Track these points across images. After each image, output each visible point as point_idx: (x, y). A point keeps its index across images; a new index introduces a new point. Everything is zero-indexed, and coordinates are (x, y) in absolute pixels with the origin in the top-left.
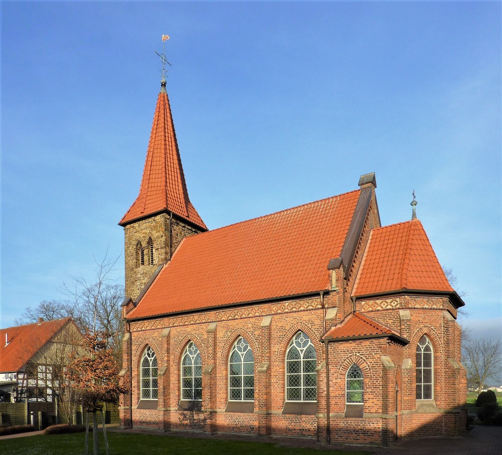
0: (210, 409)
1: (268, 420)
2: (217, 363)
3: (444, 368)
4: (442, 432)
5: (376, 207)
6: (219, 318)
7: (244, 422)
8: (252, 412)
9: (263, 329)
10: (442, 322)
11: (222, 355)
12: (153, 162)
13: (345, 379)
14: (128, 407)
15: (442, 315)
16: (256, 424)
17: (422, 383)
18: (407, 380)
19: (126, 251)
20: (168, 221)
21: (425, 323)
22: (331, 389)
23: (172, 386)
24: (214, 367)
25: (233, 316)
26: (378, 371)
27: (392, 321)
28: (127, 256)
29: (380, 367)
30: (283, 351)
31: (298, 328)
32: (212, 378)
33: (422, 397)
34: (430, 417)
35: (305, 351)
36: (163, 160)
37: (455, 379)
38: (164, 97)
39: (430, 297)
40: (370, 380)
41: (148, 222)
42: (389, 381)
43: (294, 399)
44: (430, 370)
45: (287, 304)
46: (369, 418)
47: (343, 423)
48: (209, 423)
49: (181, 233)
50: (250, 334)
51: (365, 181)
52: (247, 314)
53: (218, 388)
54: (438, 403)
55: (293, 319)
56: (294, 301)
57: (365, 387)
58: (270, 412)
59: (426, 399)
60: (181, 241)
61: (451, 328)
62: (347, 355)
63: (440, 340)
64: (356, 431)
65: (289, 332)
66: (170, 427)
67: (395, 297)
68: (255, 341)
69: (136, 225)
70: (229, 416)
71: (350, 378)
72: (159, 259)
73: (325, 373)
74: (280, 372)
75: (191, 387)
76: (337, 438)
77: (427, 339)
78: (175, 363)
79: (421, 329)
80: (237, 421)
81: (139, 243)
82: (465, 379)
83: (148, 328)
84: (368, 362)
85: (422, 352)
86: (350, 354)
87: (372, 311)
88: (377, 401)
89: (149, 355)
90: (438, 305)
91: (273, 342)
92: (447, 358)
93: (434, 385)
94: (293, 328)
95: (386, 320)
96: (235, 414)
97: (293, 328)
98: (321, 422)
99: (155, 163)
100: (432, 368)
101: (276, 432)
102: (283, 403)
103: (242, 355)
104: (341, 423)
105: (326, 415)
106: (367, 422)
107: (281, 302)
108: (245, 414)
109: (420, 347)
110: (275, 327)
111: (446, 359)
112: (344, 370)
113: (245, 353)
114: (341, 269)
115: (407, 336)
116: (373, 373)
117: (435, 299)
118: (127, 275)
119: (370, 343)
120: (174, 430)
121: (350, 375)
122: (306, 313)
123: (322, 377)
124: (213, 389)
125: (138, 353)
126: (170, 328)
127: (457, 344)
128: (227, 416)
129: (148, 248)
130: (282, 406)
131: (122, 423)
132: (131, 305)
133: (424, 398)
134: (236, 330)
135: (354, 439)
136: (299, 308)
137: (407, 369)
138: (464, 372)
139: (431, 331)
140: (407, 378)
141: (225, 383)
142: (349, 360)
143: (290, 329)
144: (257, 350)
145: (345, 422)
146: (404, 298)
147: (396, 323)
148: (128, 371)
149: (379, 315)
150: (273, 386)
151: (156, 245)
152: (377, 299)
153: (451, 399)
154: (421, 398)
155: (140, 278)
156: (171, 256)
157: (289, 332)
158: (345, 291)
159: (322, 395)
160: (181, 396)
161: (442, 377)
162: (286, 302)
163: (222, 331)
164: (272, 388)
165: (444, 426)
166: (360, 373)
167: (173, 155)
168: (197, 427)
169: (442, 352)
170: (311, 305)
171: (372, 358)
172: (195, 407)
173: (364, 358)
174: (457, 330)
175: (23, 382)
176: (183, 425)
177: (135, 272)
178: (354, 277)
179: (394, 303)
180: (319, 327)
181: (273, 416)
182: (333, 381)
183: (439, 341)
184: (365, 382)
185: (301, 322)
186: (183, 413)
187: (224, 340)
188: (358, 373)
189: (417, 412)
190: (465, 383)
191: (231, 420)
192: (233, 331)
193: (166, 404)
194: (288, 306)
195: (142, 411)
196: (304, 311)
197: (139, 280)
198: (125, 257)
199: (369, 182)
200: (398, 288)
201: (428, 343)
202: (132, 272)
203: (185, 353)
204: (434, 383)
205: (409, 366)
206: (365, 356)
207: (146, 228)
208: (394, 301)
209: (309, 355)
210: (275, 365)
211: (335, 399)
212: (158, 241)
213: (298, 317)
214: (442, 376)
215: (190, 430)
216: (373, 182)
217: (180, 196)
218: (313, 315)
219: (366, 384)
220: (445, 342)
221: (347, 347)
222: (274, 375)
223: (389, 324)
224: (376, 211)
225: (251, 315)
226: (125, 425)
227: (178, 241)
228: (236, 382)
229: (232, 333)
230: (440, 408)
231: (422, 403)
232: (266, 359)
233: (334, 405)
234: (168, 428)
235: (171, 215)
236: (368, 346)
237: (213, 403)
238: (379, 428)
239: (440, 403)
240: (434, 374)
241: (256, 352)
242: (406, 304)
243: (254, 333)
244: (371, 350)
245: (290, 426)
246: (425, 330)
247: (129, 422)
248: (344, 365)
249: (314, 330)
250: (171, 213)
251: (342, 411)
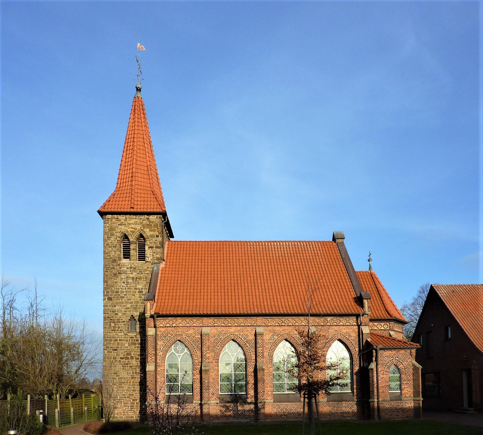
11: (268, 355)
22: (380, 382)
45: (329, 319)
69: (122, 218)
72: (153, 257)
76: (384, 416)
86: (392, 359)
96: (283, 403)
113: (182, 354)
118: (107, 265)
136: (339, 323)
155: (126, 271)
170: (348, 322)
176: (226, 416)
179: (386, 326)
182: (381, 376)
186: (225, 405)
192: (280, 335)
194: (330, 321)
196: (343, 325)
197: (125, 273)
202: (115, 264)
233: (382, 392)
248: (388, 366)
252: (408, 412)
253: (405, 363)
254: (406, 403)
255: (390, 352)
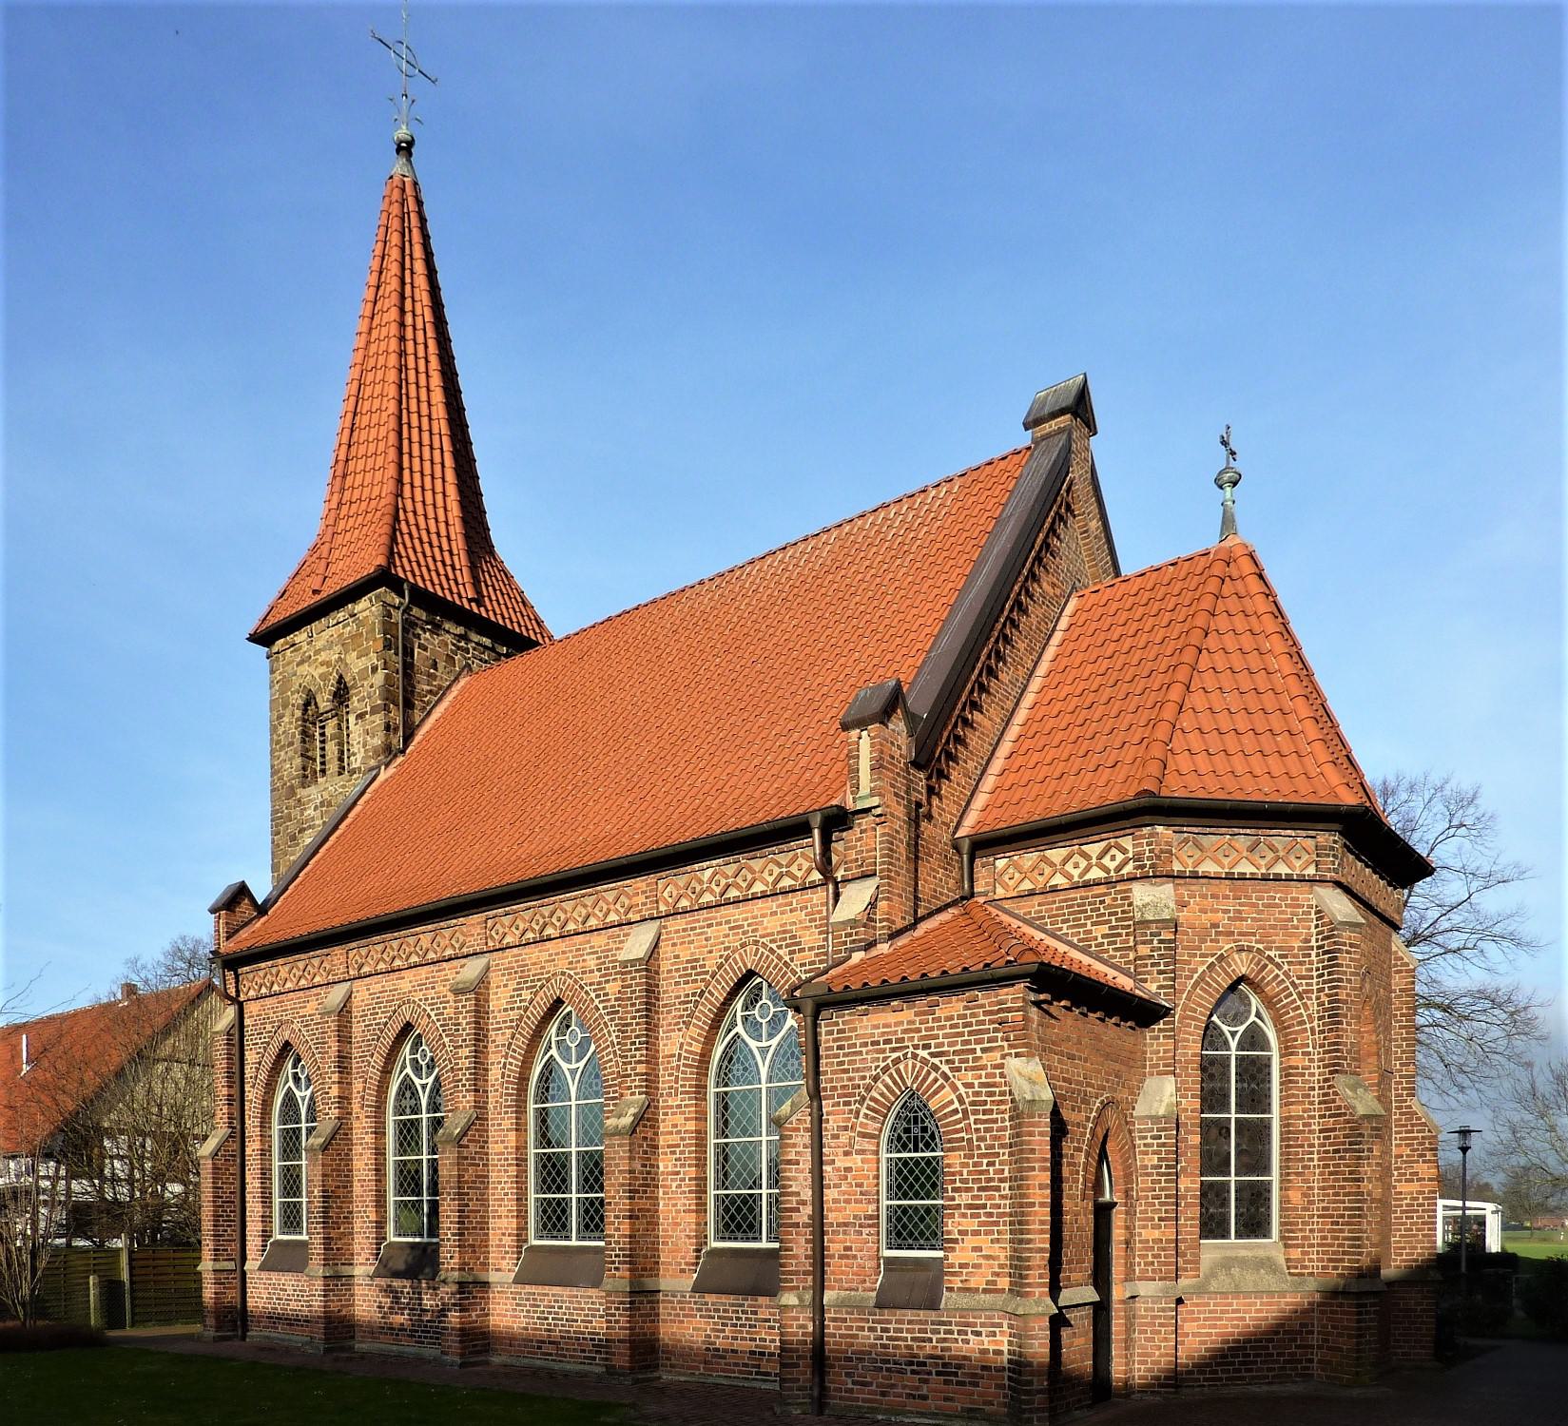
0: (456, 1273)
1: (641, 1316)
2: (490, 1106)
3: (1321, 1117)
4: (1308, 1368)
5: (1094, 507)
6: (496, 937)
7: (559, 1319)
8: (596, 1284)
9: (626, 973)
10: (1314, 931)
11: (503, 1073)
12: (358, 418)
13: (877, 1153)
14: (231, 1265)
15: (1314, 903)
16: (599, 1325)
17: (1229, 1175)
18: (1156, 1162)
19: (274, 729)
20: (397, 616)
21: (1241, 934)
22: (830, 1194)
23: (357, 1189)
24: (477, 1118)
25: (537, 928)
26: (995, 1121)
27: (1105, 929)
28: (276, 745)
29: (1002, 1102)
30: (696, 1054)
31: (745, 965)
32: (466, 1158)
33: (1229, 1232)
34: (1257, 1311)
35: (776, 1053)
36: (392, 407)
37: (1360, 1158)
38: (404, 190)
39: (1260, 832)
40: (965, 1156)
41: (335, 622)
42: (1028, 1160)
43: (740, 1235)
44: (1266, 1126)
45: (708, 873)
46: (964, 1312)
47: (871, 1329)
48: (456, 1323)
49: (450, 660)
50: (593, 995)
51: (1047, 410)
52: (580, 920)
53: (493, 1194)
54: (1296, 1254)
55: (731, 929)
56: (731, 859)
57: (950, 1187)
58: (649, 1284)
59: (1248, 1237)
60: (449, 687)
61: (1348, 952)
62: (885, 1059)
63: (1305, 1004)
64: (916, 1365)
65: (717, 981)
66: (353, 1337)
67: (1117, 833)
68: (607, 1018)
70: (528, 1300)
71: (899, 1151)
73: (806, 1130)
74: (686, 1132)
75: (419, 1194)
76: (851, 1391)
77: (1255, 1002)
78: (368, 1106)
79: (1221, 958)
80: (550, 1317)
81: (310, 701)
82: (1429, 1161)
83: (289, 985)
84: (959, 1084)
85: (1233, 1053)
86: (895, 1055)
87: (1032, 893)
88: (992, 1241)
89: (296, 1079)
90: (1298, 864)
91: (665, 1019)
92: (1331, 1072)
93: (1281, 1182)
94: (730, 965)
95: (1085, 925)
96: (547, 1289)
97: (730, 965)
98: (791, 1326)
99: (365, 420)
100: (1275, 1115)
101: (673, 1362)
102: (698, 1251)
103: (573, 1072)
104: (862, 1329)
105: (808, 1297)
106: (955, 1328)
107: (688, 868)
108: (575, 1291)
109: (1222, 1034)
110: (672, 964)
111: (1326, 1080)
112: (873, 1119)
114: (898, 725)
115: (1160, 987)
116: (977, 1130)
117: (1282, 838)
119: (966, 1008)
120: (361, 1346)
121: (899, 1138)
122: (772, 904)
123: (794, 1145)
124: (471, 1200)
125: (263, 1076)
126: (349, 983)
127: (1401, 1027)
128: (521, 1299)
129: (337, 715)
130: (693, 1264)
131: (210, 1321)
132: (244, 908)
133: (1239, 1236)
134: (548, 980)
135: (909, 1396)
137: (1155, 1119)
138: (1427, 1134)
139: (1265, 966)
140: (1154, 1153)
141: (513, 1176)
142: (891, 1076)
143: (719, 968)
144: (615, 1052)
145: (879, 1326)
146: (1151, 835)
147: (1120, 935)
148: (230, 1136)
149: (1057, 909)
150: (663, 1186)
151: (358, 701)
152: (1052, 845)
153: (1345, 1239)
154: (1225, 1235)
155: (313, 819)
156: (408, 738)
157: (717, 981)
158: (918, 815)
159: (796, 1217)
160: (390, 1228)
161: (1312, 1153)
162: (705, 864)
163: (505, 986)
164: (661, 1194)
165: (1320, 1347)
166: (934, 1128)
167: (432, 388)
168: (431, 1338)
169: (1310, 1049)
170: (789, 874)
171: (973, 1069)
172: (421, 1263)
173: (945, 1068)
174: (1400, 971)
175: (54, 1186)
177: (299, 801)
178: (971, 765)
179: (1113, 858)
180: (817, 955)
181: (664, 1301)
182: (838, 1164)
183: (1298, 1008)
184: (949, 1166)
185: (756, 942)
186: (390, 1286)
187: (512, 1021)
188: (924, 1130)
189: (1201, 1290)
190: (1430, 1180)
191: (534, 1312)
193: (336, 1253)
195: (274, 1275)
196: (764, 896)
197: (310, 827)
198: (272, 751)
199: (1062, 412)
200: (1114, 790)
201: (1258, 1015)
202: (292, 802)
203: (401, 1072)
204: (1281, 1175)
205: (1164, 1104)
206: (947, 1062)
207: (330, 646)
208: (1114, 851)
209: (789, 1067)
210: (671, 1107)
211: (845, 1233)
212: (363, 686)
213: (746, 923)
214: (1313, 1146)
215: (410, 1348)
216: (1080, 407)
217: (451, 528)
218: (795, 910)
219: (953, 1174)
220: (1325, 1010)
221: (886, 1026)
222: (669, 1146)
223: (1093, 943)
224: (1094, 524)
225: (593, 922)
226: (218, 1328)
227: (440, 687)
228: (553, 1173)
229: (536, 994)
230: (1303, 1274)
231: (1229, 1253)
232: (637, 1083)
233: (841, 1257)
234: (346, 1338)
235: (406, 592)
236: (960, 1017)
237: (474, 1252)
238: (998, 1352)
239: (1304, 1253)
240: (1282, 1140)
241: (611, 1060)
242: (1158, 857)
243: (604, 988)
244: (970, 1033)
245: (718, 1337)
246: (1241, 965)
247: (236, 1317)
248: (873, 1099)
249: (798, 970)
250: (405, 586)
251: (868, 1284)
252: (977, 1385)
253: (969, 1077)
254: (968, 1325)
255: (890, 1017)
